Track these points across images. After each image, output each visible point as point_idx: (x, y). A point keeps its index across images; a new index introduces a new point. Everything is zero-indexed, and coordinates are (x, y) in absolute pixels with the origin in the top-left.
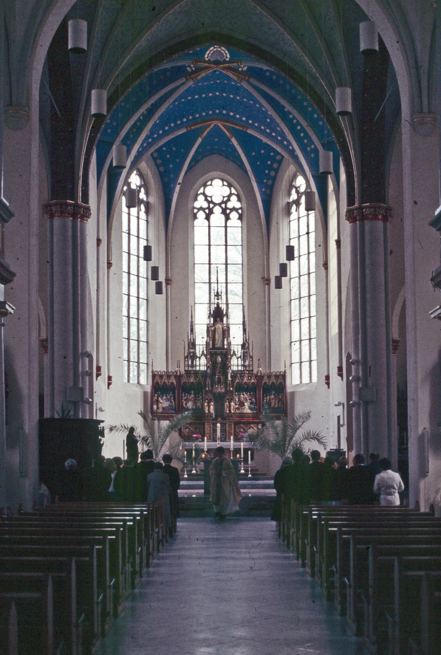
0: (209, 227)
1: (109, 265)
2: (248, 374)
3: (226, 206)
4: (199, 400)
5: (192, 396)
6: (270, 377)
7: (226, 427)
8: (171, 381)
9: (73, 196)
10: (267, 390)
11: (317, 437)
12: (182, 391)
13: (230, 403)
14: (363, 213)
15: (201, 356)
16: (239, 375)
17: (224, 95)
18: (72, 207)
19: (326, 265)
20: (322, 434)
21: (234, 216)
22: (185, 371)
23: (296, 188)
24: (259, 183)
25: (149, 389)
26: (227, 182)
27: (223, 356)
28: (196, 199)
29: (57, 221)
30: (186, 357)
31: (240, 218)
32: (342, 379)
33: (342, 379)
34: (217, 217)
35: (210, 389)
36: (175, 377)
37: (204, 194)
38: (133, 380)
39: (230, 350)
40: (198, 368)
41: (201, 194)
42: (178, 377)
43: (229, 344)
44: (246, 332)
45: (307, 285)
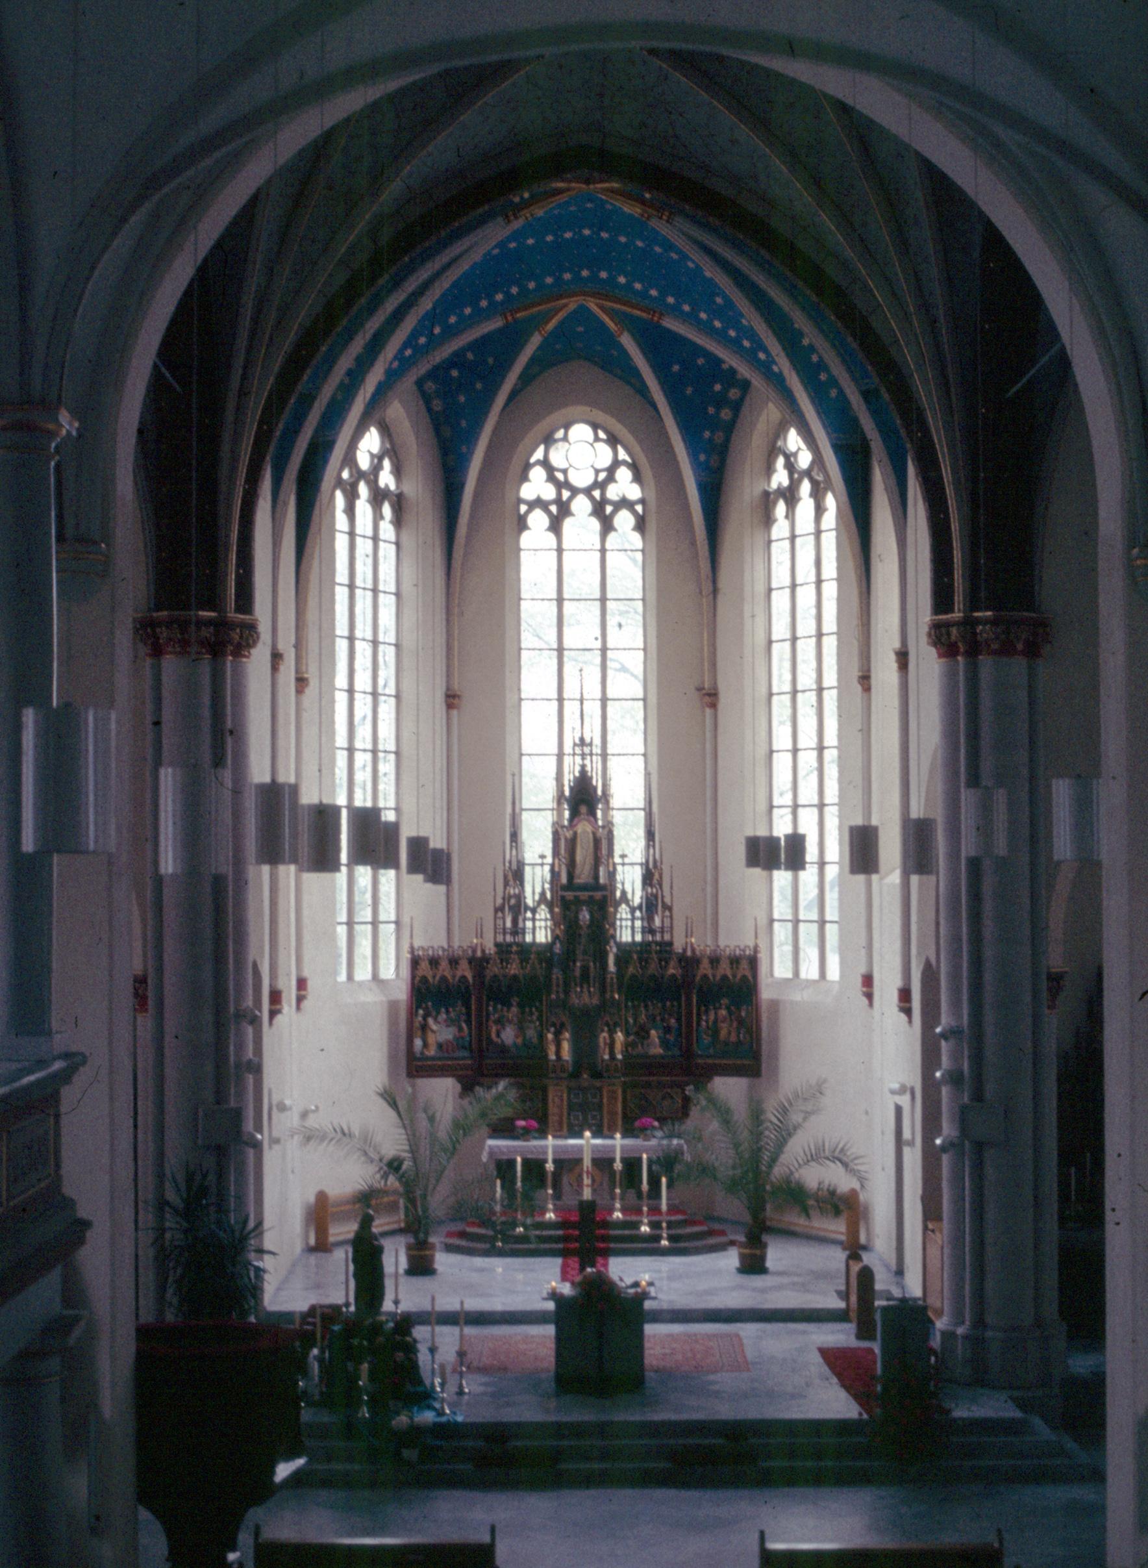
0: (560, 550)
1: (301, 682)
3: (603, 494)
5: (514, 1009)
8: (459, 973)
9: (213, 600)
11: (841, 1156)
12: (489, 999)
13: (612, 1033)
14: (975, 634)
16: (635, 956)
17: (605, 235)
18: (212, 629)
19: (865, 679)
20: (853, 1151)
21: (624, 520)
22: (497, 945)
23: (787, 457)
24: (693, 450)
25: (402, 993)
26: (606, 431)
28: (524, 477)
29: (170, 663)
30: (499, 909)
31: (641, 525)
32: (910, 1021)
33: (910, 1021)
34: (581, 524)
35: (562, 996)
36: (470, 963)
37: (545, 463)
38: (363, 973)
39: (613, 889)
40: (528, 938)
41: (538, 462)
42: (479, 963)
43: (612, 875)
44: (654, 841)
45: (813, 664)
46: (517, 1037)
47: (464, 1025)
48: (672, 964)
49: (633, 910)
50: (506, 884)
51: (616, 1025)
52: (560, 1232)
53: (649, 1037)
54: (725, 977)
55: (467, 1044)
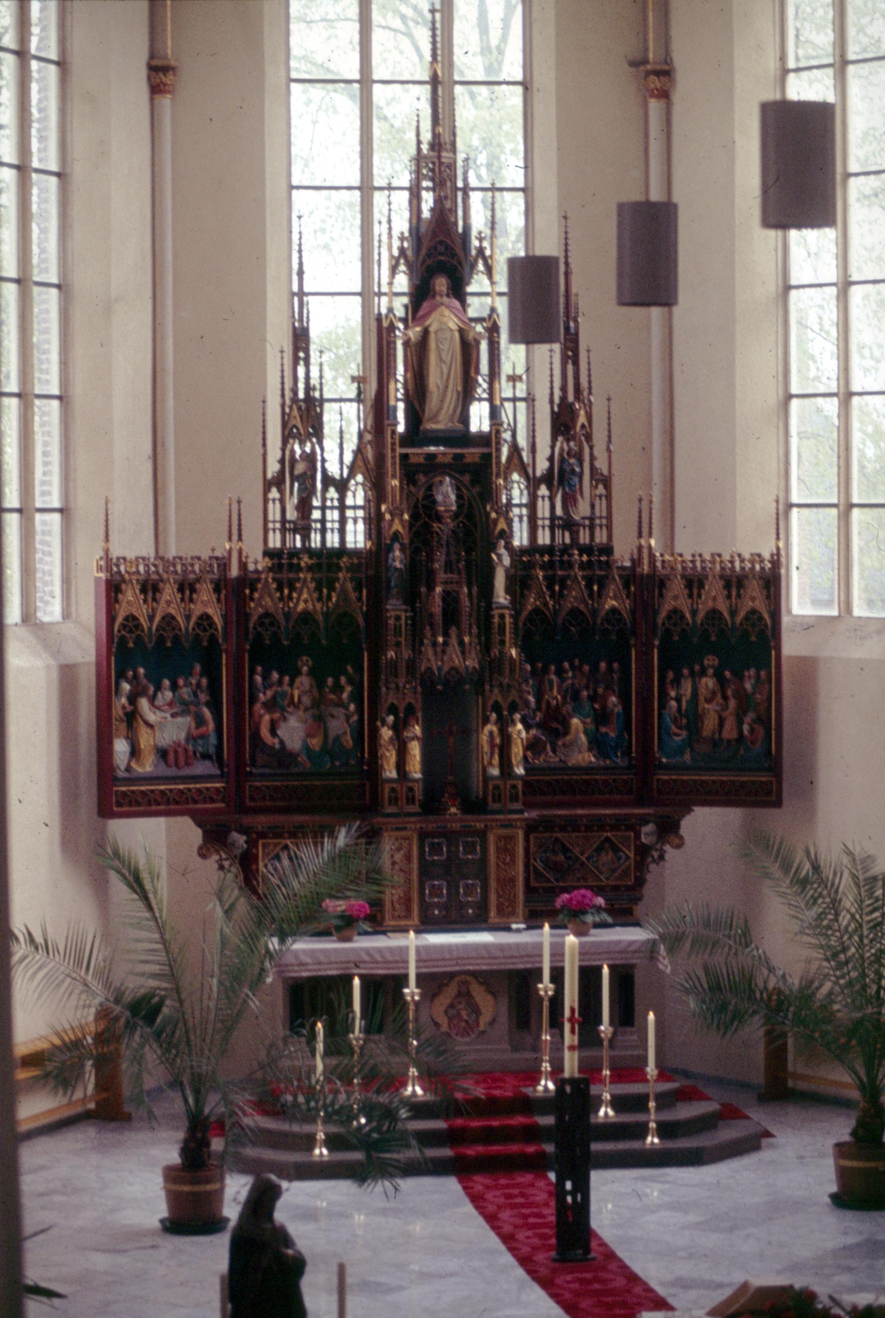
2: (588, 566)
4: (341, 704)
5: (304, 681)
6: (701, 585)
7: (485, 849)
8: (197, 610)
10: (684, 646)
12: (254, 661)
13: (504, 724)
15: (352, 474)
22: (269, 553)
27: (467, 478)
35: (407, 654)
36: (217, 590)
40: (333, 540)
42: (236, 588)
46: (309, 735)
47: (207, 713)
48: (611, 590)
49: (533, 483)
50: (287, 437)
51: (513, 708)
52: (440, 1124)
53: (566, 732)
54: (714, 614)
55: (212, 750)
